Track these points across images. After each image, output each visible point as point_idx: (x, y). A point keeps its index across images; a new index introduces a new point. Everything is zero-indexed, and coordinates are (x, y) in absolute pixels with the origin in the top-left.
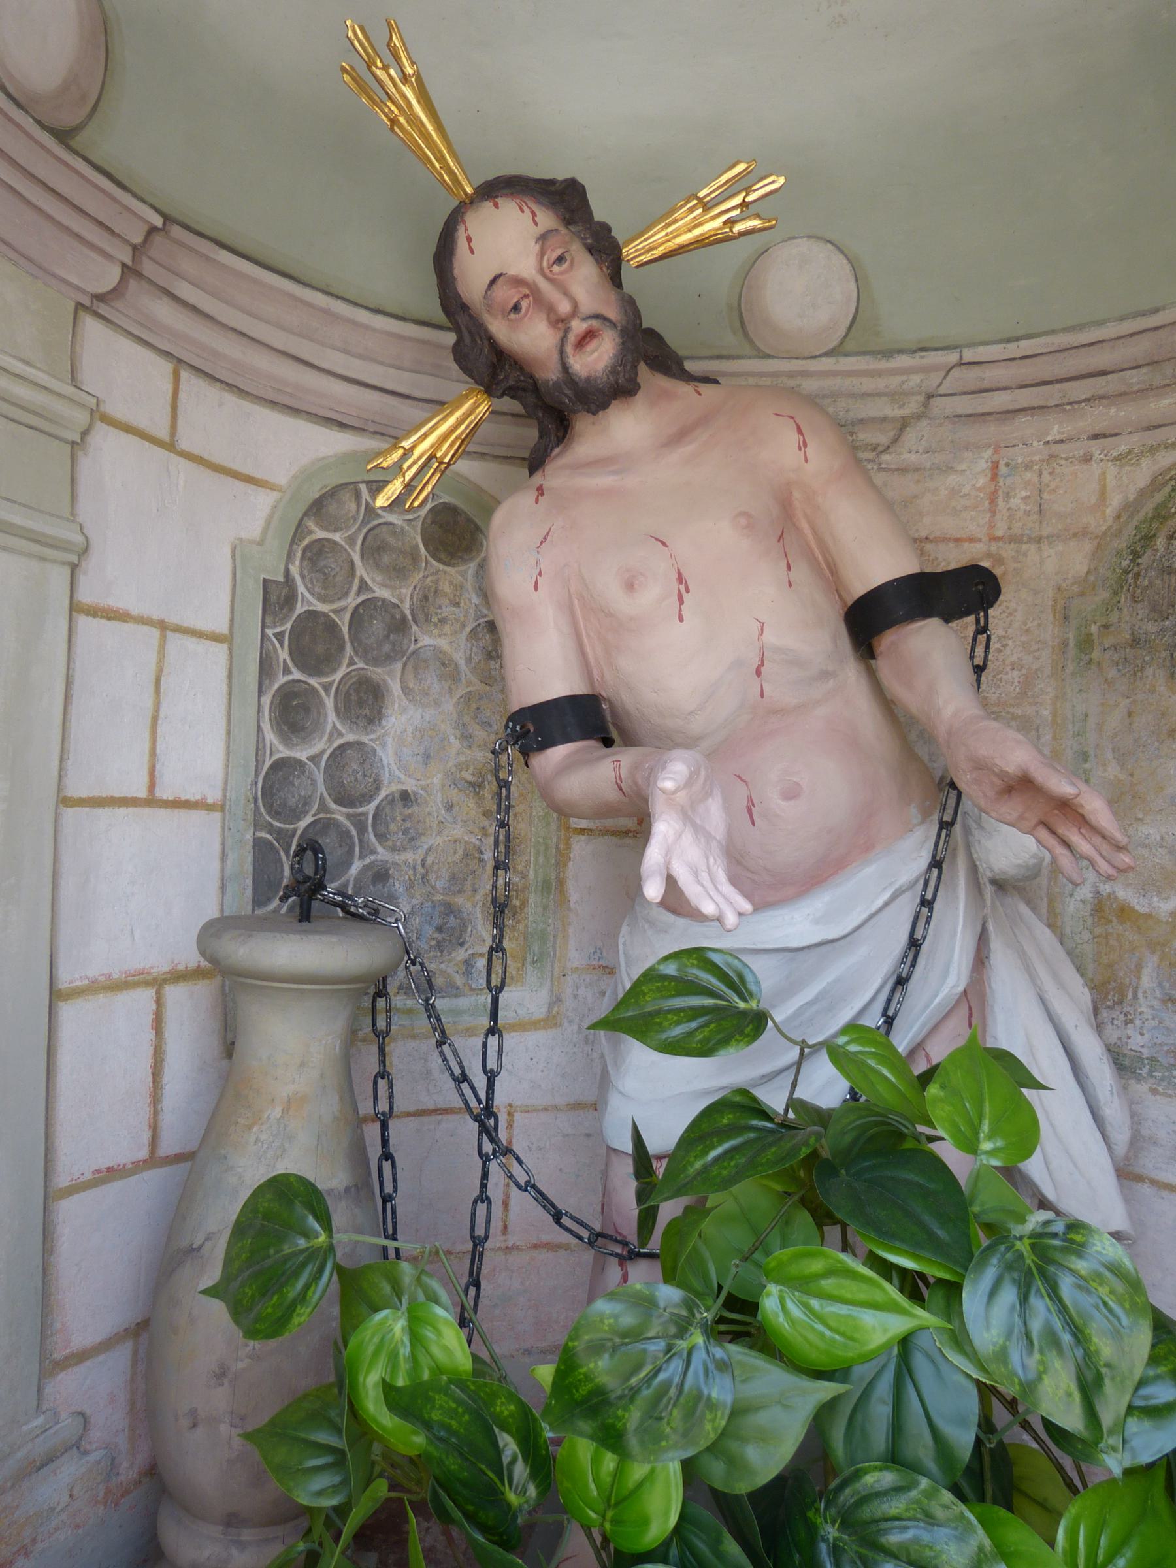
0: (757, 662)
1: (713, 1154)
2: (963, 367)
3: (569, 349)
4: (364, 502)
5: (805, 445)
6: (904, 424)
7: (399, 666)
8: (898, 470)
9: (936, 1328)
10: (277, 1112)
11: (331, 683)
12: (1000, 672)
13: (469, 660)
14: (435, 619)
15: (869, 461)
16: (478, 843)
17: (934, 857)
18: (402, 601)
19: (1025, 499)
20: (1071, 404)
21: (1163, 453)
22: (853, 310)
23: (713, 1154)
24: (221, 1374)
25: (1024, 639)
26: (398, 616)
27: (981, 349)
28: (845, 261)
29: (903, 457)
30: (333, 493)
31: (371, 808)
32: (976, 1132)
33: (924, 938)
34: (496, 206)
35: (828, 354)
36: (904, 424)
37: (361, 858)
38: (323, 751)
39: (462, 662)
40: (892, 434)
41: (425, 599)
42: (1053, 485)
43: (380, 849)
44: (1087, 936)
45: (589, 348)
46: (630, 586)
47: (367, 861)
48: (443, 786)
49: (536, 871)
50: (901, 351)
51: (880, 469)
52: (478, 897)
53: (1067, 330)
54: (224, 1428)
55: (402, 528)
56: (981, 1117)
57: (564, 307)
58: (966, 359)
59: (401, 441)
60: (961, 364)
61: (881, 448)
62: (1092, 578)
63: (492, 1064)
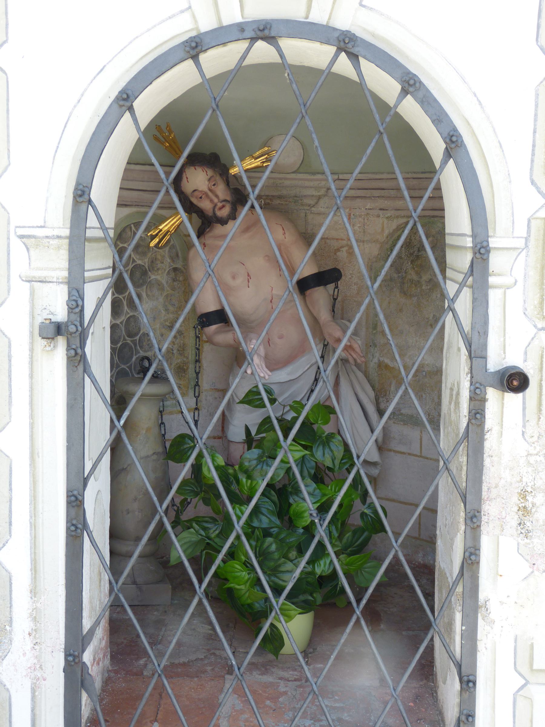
0: (270, 299)
1: (266, 427)
2: (340, 181)
3: (216, 210)
4: (133, 231)
5: (285, 234)
6: (319, 198)
7: (145, 287)
8: (317, 213)
9: (309, 454)
10: (144, 432)
11: (125, 296)
12: (351, 286)
13: (167, 282)
14: (156, 269)
15: (308, 210)
16: (172, 347)
17: (322, 355)
18: (145, 264)
19: (359, 227)
20: (373, 197)
21: (400, 219)
22: (302, 159)
23: (266, 427)
24: (135, 499)
25: (358, 275)
26: (144, 270)
27: (345, 175)
28: (299, 143)
29: (319, 209)
30: (124, 230)
31: (137, 338)
32: (318, 420)
33: (319, 378)
34: (195, 169)
35: (293, 173)
36: (319, 198)
37: (136, 355)
38: (124, 320)
39: (165, 283)
40: (315, 201)
41: (153, 262)
42: (368, 224)
43: (141, 352)
44: (376, 374)
45: (222, 210)
46: (234, 278)
47: (137, 356)
48: (160, 328)
49: (192, 356)
50: (318, 173)
51: (311, 213)
52: (172, 366)
53: (373, 173)
54: (137, 513)
55: (145, 238)
56: (319, 417)
57: (216, 200)
58: (340, 178)
59: (159, 226)
60: (338, 179)
61: (311, 206)
62: (379, 256)
63: (196, 418)
